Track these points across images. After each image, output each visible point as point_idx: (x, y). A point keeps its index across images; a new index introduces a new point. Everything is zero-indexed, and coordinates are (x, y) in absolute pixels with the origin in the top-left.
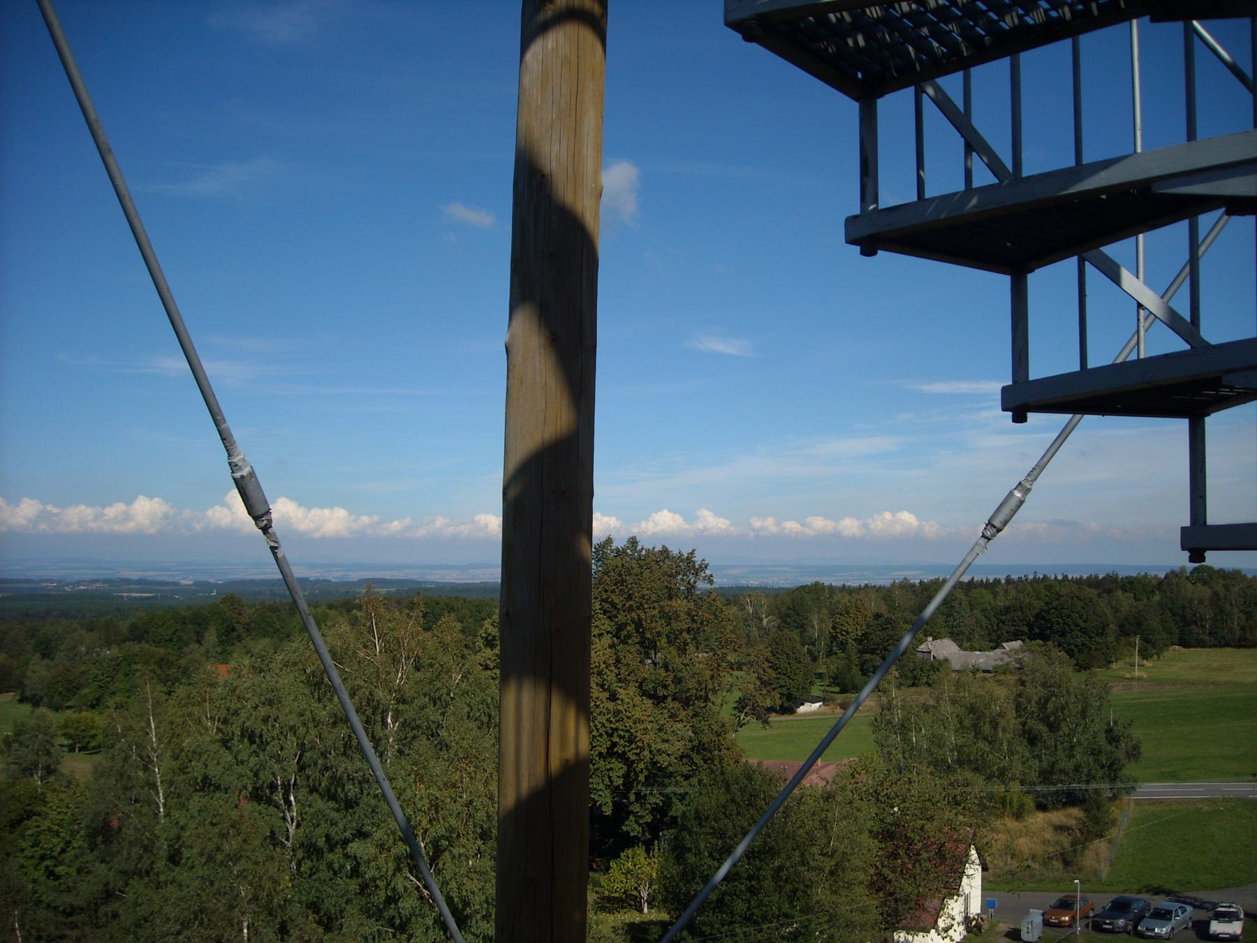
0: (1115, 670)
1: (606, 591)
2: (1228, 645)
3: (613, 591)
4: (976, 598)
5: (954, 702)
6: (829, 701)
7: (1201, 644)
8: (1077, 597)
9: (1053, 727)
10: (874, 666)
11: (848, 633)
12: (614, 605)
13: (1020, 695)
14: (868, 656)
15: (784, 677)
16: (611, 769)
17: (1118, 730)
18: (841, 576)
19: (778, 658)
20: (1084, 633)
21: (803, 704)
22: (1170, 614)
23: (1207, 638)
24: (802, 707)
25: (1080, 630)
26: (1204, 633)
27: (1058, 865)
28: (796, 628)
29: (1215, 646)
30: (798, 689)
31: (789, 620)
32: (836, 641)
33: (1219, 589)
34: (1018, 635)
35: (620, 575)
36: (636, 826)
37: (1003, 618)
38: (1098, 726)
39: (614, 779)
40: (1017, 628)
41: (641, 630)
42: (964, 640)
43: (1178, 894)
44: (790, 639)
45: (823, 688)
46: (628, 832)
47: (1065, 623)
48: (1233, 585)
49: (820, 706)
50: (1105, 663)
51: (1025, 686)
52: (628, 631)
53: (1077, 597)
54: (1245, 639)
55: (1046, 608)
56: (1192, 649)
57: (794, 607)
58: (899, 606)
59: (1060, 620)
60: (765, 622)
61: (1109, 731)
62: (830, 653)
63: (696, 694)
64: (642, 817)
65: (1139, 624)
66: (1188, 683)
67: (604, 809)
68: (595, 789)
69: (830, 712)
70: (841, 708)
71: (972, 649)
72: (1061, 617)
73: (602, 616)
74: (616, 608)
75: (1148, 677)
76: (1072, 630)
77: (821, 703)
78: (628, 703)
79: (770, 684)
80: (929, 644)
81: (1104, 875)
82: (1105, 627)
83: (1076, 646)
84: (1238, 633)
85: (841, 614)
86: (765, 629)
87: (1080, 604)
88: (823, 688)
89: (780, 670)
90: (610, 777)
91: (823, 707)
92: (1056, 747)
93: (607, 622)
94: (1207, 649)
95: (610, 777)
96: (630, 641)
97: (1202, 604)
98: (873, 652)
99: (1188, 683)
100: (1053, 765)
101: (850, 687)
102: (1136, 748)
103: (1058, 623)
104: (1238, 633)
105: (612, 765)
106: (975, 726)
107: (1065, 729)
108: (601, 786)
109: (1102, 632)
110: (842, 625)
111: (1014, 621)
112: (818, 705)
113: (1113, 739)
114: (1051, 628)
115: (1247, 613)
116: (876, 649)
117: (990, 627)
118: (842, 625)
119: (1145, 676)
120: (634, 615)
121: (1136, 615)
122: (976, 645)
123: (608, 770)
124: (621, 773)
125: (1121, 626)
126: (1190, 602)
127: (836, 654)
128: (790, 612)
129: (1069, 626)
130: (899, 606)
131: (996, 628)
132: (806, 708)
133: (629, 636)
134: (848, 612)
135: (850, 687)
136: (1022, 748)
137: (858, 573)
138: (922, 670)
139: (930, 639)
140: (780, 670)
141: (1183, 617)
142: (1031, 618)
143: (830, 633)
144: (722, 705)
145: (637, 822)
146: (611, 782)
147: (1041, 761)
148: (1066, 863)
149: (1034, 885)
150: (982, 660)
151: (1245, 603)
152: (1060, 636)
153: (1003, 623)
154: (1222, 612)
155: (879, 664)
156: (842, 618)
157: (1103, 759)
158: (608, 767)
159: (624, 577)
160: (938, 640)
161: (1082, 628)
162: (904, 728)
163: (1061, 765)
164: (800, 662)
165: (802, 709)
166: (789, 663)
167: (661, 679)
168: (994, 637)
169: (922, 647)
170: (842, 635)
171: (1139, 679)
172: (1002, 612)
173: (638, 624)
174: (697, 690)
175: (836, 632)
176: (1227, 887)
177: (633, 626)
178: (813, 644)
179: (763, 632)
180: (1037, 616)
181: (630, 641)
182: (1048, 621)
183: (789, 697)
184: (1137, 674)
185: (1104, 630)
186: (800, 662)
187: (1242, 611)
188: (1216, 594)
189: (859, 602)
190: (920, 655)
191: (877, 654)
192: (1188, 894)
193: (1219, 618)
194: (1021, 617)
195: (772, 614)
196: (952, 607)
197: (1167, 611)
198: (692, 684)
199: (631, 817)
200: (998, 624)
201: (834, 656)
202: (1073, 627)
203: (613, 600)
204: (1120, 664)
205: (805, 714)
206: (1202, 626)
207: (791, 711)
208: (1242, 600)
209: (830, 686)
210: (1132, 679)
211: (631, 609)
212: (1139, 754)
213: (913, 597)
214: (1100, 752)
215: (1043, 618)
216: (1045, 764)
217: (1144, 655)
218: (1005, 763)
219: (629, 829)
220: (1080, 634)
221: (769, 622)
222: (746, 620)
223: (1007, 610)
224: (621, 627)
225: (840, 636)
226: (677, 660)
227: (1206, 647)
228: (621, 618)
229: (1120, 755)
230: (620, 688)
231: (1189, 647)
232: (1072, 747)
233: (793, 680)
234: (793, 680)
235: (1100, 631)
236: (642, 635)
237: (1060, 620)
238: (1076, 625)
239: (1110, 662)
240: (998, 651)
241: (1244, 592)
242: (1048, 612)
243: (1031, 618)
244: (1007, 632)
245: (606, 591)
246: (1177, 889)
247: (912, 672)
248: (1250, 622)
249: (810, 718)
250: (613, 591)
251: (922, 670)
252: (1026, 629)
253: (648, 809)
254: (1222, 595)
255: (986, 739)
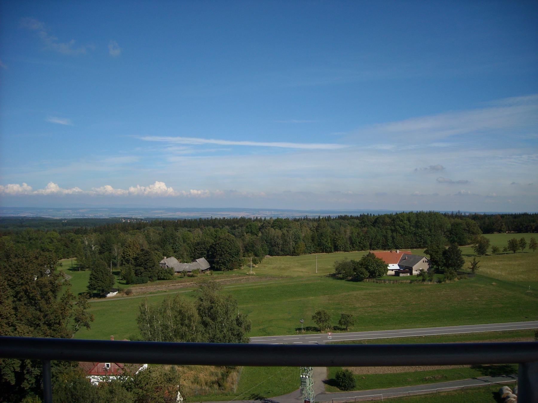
0: (243, 270)
1: (10, 275)
2: (288, 255)
3: (14, 276)
4: (185, 236)
5: (172, 309)
6: (120, 291)
7: (278, 254)
8: (227, 239)
9: (214, 319)
10: (141, 272)
11: (129, 255)
12: (14, 283)
13: (200, 305)
14: (138, 268)
15: (100, 282)
16: (14, 363)
17: (242, 319)
18: (130, 213)
19: (98, 274)
20: (230, 255)
21: (109, 293)
22: (265, 242)
23: (280, 252)
24: (109, 294)
25: (228, 254)
26: (279, 250)
27: (216, 386)
28: (107, 250)
29: (283, 255)
30: (107, 287)
31: (104, 247)
32: (125, 260)
33: (285, 232)
34: (202, 254)
35: (17, 268)
36: (28, 385)
37: (197, 247)
38: (233, 317)
39: (16, 368)
40: (202, 251)
41: (27, 294)
42: (181, 258)
43: (265, 399)
44: (103, 265)
45: (119, 281)
46: (24, 388)
47: (222, 251)
48: (290, 230)
49: (117, 294)
50: (239, 267)
51: (203, 302)
52: (21, 295)
53: (227, 239)
54: (295, 252)
55: (214, 243)
56: (274, 257)
57: (106, 241)
58: (153, 240)
59: (220, 250)
60: (93, 248)
61: (237, 320)
62: (122, 264)
63: (54, 322)
64: (30, 381)
65: (253, 246)
66: (272, 277)
67: (11, 382)
68: (6, 374)
69: (121, 296)
70: (126, 294)
71: (184, 262)
72: (221, 248)
73: (8, 288)
74: (15, 284)
75: (256, 273)
76: (225, 254)
77: (117, 292)
78: (21, 333)
79: (94, 285)
80: (165, 260)
81: (235, 391)
82: (238, 252)
83: (227, 260)
84: (292, 250)
85: (127, 247)
86: (93, 252)
87: (228, 242)
88: (119, 281)
89: (98, 279)
90: (13, 367)
91: (118, 294)
92: (215, 328)
93: (11, 290)
94: (280, 257)
95: (13, 367)
96: (22, 299)
97: (278, 238)
98: (140, 266)
99: (272, 277)
100: (215, 336)
101: (130, 282)
102: (249, 326)
103: (219, 251)
104: (292, 250)
105: (14, 362)
106: (182, 320)
107: (219, 320)
108: (10, 372)
109: (237, 254)
110: (127, 252)
111: (201, 248)
112: (116, 293)
113: (239, 324)
114: (216, 252)
115: (295, 241)
116: (142, 264)
117: (191, 251)
118: (127, 252)
119: (255, 274)
120: (23, 287)
121: (252, 242)
122: (185, 260)
123: (12, 364)
124: (19, 365)
125: (246, 247)
126: (274, 237)
127: (125, 264)
128: (105, 243)
129: (223, 252)
130: (153, 240)
131: (193, 251)
132: (111, 295)
133: (22, 297)
134: (130, 247)
135: (130, 282)
136: (202, 328)
137: (138, 212)
138: (162, 273)
139: (165, 258)
140: (98, 279)
141: (271, 243)
142: (209, 248)
143: (122, 255)
144: (67, 323)
145: (28, 383)
146: (14, 369)
147: (209, 334)
148: (220, 386)
149: (206, 398)
150: (187, 267)
151: (295, 238)
152: (220, 256)
153: (197, 250)
154: (286, 241)
155: (143, 271)
156: (127, 249)
157: (235, 333)
158: (13, 363)
159: (19, 268)
160: (169, 258)
161: (229, 253)
162: (150, 321)
163: (218, 336)
164: (108, 275)
165: (109, 295)
166: (103, 276)
167: (38, 316)
168: (193, 255)
169: (162, 262)
170: (127, 256)
171: (252, 275)
172: (196, 245)
173: (26, 291)
174: (54, 319)
175: (125, 255)
176: (284, 394)
177: (24, 292)
178: (115, 259)
179: (92, 252)
180: (211, 247)
181: (22, 299)
182: (215, 249)
183: (103, 291)
184: (251, 272)
185: (238, 253)
186: (108, 275)
187: (294, 241)
188: (283, 234)
189: (134, 242)
190: (161, 265)
191: (143, 266)
192: (269, 399)
193: (285, 243)
194: (204, 247)
195: (97, 244)
196: (176, 240)
197: (264, 241)
198: (52, 317)
199: (26, 381)
200: (195, 249)
201: (124, 266)
202: (225, 252)
203: (13, 280)
204: (245, 266)
205: (110, 298)
206: (278, 247)
207: (104, 296)
208: (294, 236)
209: (121, 279)
210: (249, 275)
211: (22, 284)
212: (250, 329)
213: (159, 236)
214: (234, 330)
215: (213, 248)
216: (211, 335)
217: (255, 262)
218: (194, 336)
219: (24, 386)
220: (228, 255)
221: (95, 248)
222: (84, 248)
223: (198, 244)
224: (18, 293)
225: (126, 257)
226: (45, 306)
227: (279, 256)
228: (18, 289)
229: (242, 330)
230: (18, 323)
231: (273, 256)
232: (222, 327)
233: (105, 283)
234: (105, 283)
235: (237, 253)
236: (28, 296)
237: (220, 250)
238: (227, 251)
239: (240, 266)
240: (194, 263)
241: (294, 233)
242: (215, 245)
243: (209, 248)
244: (198, 253)
245: (10, 275)
246: (264, 396)
247: (157, 274)
248: (297, 245)
249: (112, 300)
250: (14, 276)
251: (162, 273)
252: (206, 252)
253: (33, 377)
254: (286, 235)
255: (186, 325)
